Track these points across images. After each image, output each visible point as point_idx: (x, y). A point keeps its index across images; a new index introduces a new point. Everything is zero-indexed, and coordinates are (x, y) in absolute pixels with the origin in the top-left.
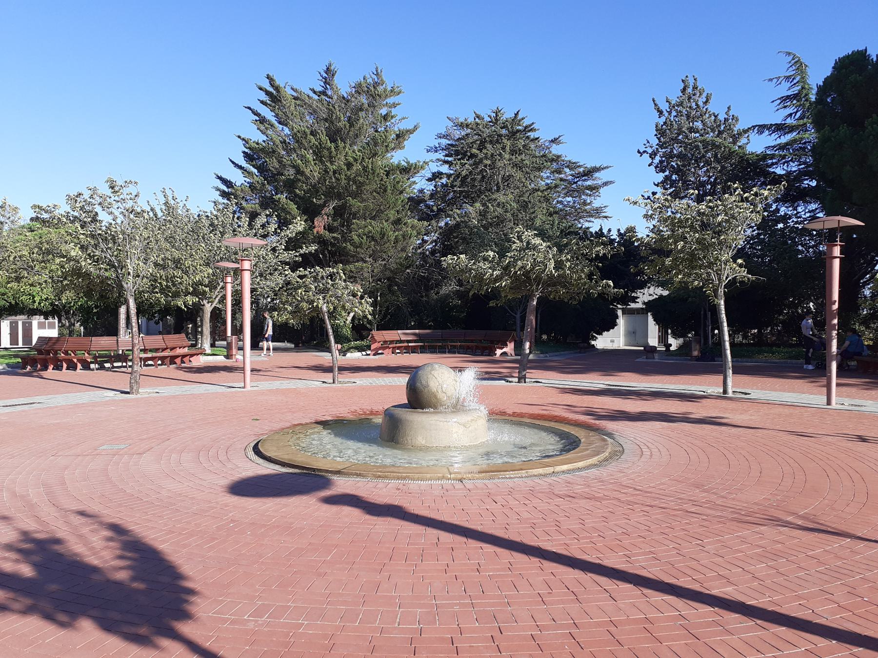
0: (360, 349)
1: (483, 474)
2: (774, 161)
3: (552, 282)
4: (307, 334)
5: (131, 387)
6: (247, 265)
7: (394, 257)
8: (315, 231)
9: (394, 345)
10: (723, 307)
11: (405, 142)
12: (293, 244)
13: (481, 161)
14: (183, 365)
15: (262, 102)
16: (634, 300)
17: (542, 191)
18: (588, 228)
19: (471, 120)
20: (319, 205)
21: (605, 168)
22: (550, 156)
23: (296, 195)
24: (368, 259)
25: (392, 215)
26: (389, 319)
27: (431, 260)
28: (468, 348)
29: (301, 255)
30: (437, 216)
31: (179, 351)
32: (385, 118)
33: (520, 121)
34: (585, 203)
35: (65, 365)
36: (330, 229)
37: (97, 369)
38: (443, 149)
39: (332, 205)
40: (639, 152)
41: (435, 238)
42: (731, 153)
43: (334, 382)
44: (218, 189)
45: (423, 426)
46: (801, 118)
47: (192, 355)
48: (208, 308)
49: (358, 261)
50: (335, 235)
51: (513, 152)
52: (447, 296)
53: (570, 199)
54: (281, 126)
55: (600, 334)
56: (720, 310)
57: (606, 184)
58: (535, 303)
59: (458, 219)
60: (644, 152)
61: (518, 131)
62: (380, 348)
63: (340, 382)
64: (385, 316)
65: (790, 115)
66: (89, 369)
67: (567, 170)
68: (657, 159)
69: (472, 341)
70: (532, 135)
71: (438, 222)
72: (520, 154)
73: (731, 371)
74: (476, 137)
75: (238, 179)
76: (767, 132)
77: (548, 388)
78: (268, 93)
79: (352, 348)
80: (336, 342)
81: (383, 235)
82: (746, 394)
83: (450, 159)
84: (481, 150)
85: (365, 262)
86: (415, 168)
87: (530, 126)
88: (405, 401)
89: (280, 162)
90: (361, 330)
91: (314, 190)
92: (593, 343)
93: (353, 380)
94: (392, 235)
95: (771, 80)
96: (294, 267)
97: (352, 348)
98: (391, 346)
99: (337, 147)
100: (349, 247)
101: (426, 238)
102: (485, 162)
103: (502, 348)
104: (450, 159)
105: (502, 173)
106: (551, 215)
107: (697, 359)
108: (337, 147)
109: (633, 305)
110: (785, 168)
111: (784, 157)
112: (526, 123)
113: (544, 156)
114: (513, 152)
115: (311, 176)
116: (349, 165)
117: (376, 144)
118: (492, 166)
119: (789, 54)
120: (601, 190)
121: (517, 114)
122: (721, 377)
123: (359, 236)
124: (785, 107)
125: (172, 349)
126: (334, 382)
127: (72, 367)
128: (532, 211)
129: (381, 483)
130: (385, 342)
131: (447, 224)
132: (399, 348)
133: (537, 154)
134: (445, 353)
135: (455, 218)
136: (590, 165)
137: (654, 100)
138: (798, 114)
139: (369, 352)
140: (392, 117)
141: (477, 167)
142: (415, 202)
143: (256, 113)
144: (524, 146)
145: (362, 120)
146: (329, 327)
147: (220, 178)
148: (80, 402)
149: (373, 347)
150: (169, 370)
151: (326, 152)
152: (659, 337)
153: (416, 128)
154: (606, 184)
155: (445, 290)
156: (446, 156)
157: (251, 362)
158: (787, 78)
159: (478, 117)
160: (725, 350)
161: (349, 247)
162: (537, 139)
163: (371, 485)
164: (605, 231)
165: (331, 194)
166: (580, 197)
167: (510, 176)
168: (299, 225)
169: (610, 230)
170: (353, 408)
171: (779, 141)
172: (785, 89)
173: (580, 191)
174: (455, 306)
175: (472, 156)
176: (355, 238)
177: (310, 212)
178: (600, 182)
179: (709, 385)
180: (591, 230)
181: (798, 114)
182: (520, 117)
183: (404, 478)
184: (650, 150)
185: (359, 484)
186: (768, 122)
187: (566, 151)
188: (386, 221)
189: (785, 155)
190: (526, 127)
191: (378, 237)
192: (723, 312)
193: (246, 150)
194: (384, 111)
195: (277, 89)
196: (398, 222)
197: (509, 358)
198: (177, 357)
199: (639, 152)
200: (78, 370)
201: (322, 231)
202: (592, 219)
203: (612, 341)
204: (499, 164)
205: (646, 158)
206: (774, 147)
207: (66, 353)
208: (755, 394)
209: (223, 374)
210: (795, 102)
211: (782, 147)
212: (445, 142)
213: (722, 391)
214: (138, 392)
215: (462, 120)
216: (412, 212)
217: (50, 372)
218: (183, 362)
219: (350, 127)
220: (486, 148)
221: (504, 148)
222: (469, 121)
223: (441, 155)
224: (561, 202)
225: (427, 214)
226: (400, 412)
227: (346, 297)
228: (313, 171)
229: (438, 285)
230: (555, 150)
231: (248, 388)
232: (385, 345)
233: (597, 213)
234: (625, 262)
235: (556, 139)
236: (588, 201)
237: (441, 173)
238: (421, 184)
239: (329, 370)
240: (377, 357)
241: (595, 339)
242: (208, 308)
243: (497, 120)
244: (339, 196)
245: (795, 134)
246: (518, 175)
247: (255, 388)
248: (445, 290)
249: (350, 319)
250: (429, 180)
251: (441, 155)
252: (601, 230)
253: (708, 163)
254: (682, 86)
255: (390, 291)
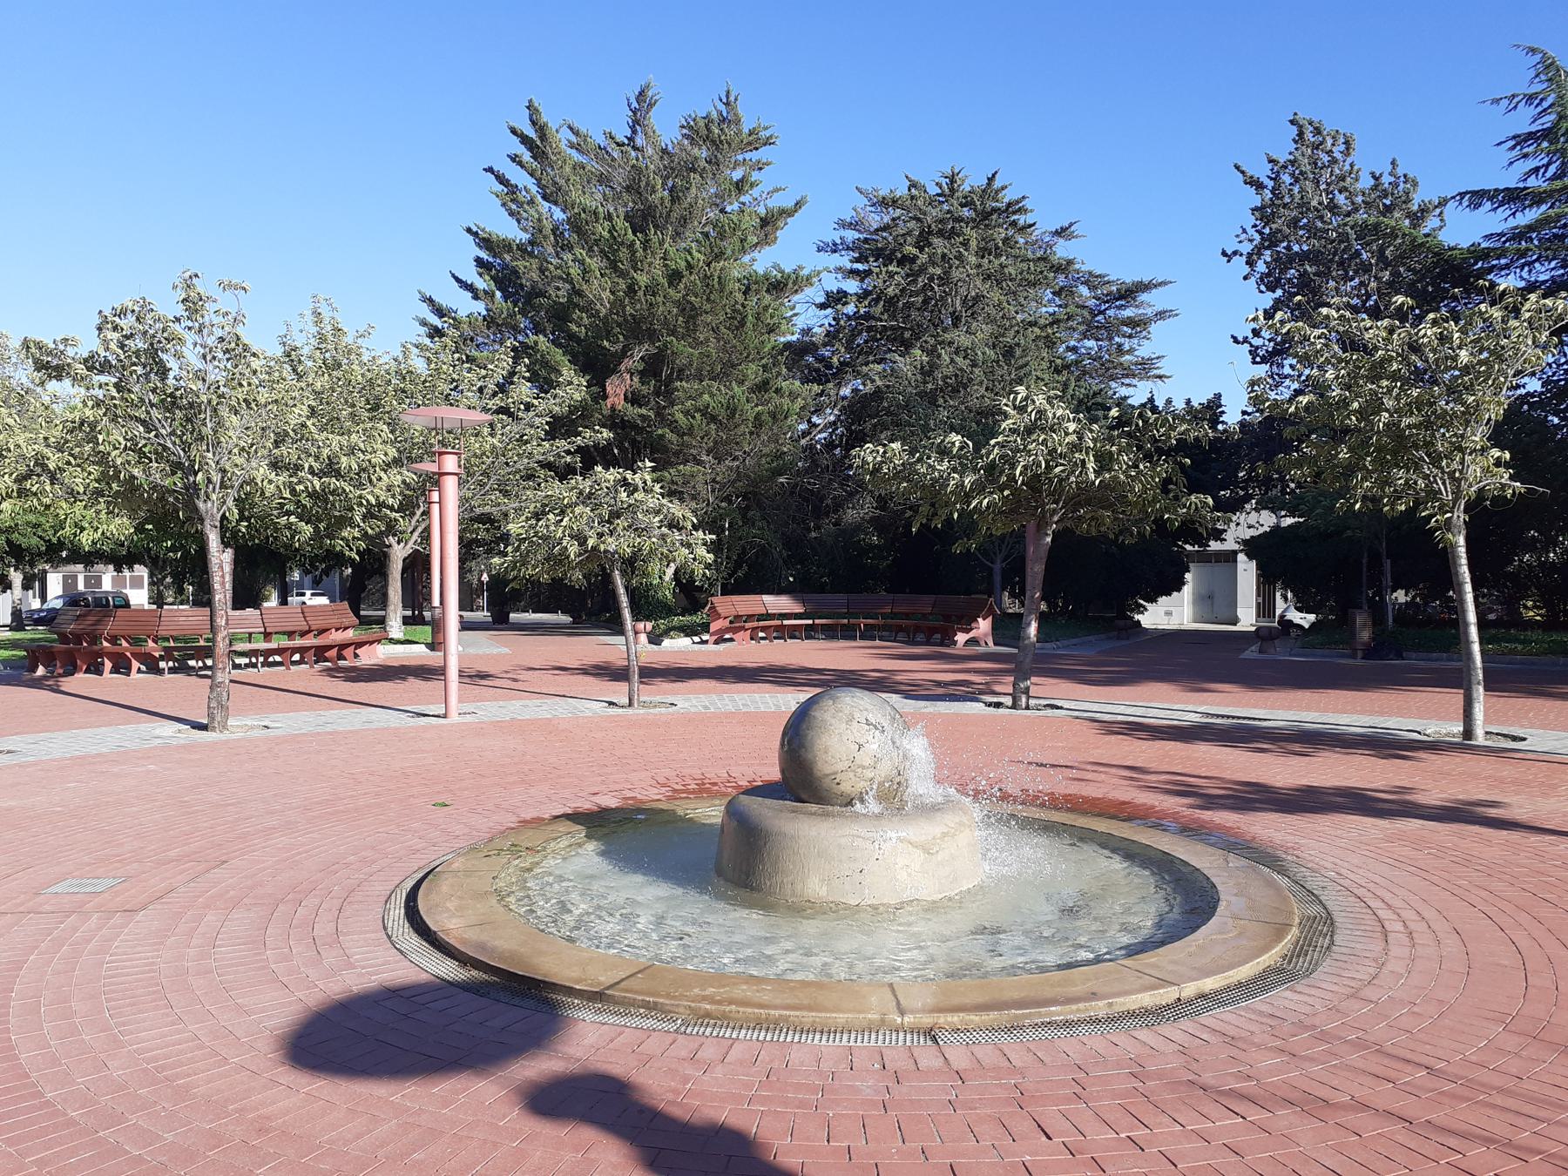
0: (689, 631)
1: (993, 1015)
2: (1503, 261)
3: (1086, 496)
4: (586, 599)
5: (211, 716)
6: (450, 463)
7: (753, 450)
8: (609, 402)
9: (755, 624)
10: (1462, 551)
11: (779, 233)
12: (559, 427)
13: (923, 269)
14: (341, 663)
15: (515, 159)
16: (1218, 535)
17: (1043, 328)
18: (1126, 398)
19: (902, 191)
20: (614, 355)
21: (1160, 284)
22: (1055, 259)
23: (572, 336)
24: (704, 458)
25: (753, 371)
26: (746, 571)
27: (830, 462)
28: (900, 629)
29: (580, 450)
30: (839, 374)
31: (336, 637)
32: (740, 186)
33: (997, 192)
34: (1120, 350)
35: (108, 665)
36: (634, 399)
37: (172, 670)
38: (848, 248)
39: (639, 352)
40: (1224, 254)
41: (832, 418)
42: (1416, 247)
43: (630, 705)
44: (424, 323)
45: (827, 855)
46: (1555, 177)
47: (360, 645)
48: (399, 553)
49: (685, 462)
50: (644, 411)
51: (982, 252)
52: (858, 528)
53: (1091, 343)
54: (546, 204)
55: (1153, 600)
56: (1455, 557)
57: (1161, 315)
58: (1049, 539)
59: (879, 383)
60: (1235, 253)
61: (994, 210)
62: (728, 630)
63: (644, 705)
64: (738, 565)
65: (1537, 170)
66: (160, 672)
67: (1084, 290)
68: (1261, 267)
69: (907, 616)
70: (1022, 220)
71: (839, 385)
72: (998, 256)
73: (1481, 689)
74: (912, 224)
75: (467, 307)
76: (1488, 205)
77: (1070, 722)
78: (525, 140)
79: (673, 628)
80: (637, 617)
81: (732, 410)
82: (1515, 739)
83: (860, 266)
84: (921, 250)
85: (700, 463)
86: (795, 283)
87: (1018, 202)
88: (774, 773)
89: (542, 271)
90: (691, 595)
91: (604, 329)
92: (1137, 617)
93: (670, 699)
94: (750, 410)
95: (1497, 101)
96: (564, 473)
97: (673, 628)
98: (748, 625)
99: (646, 244)
100: (670, 436)
101: (815, 419)
102: (931, 270)
103: (967, 631)
104: (860, 266)
105: (963, 291)
106: (1057, 371)
107: (1371, 652)
108: (646, 244)
109: (1214, 546)
110: (1525, 274)
111: (1523, 254)
112: (1008, 196)
113: (1043, 259)
114: (982, 252)
115: (600, 296)
116: (674, 277)
117: (722, 236)
118: (945, 279)
119: (1533, 51)
120: (1153, 328)
121: (991, 180)
122: (1455, 697)
123: (686, 413)
124: (1525, 156)
125: (322, 632)
126: (630, 705)
127: (122, 666)
128: (1021, 362)
129: (710, 1040)
130: (738, 617)
131: (855, 391)
132: (763, 629)
133: (1030, 255)
134: (854, 638)
135: (873, 381)
136: (1129, 278)
137: (1237, 167)
138: (1552, 169)
139: (706, 637)
140: (752, 185)
141: (915, 281)
142: (799, 351)
143: (501, 179)
144: (1006, 240)
145: (693, 190)
146: (622, 590)
147: (430, 301)
148: (93, 750)
149: (714, 627)
150: (304, 675)
151: (624, 253)
152: (1258, 604)
153: (799, 205)
154: (1161, 315)
155: (851, 515)
156: (857, 260)
157: (461, 657)
158: (1530, 98)
159: (913, 185)
160: (1468, 643)
161: (670, 436)
162: (1031, 226)
163: (683, 1047)
164: (1160, 403)
165: (638, 330)
166: (1111, 339)
167: (978, 298)
168: (573, 387)
169: (1169, 401)
170: (664, 773)
171: (1512, 223)
172: (1524, 120)
173: (1110, 329)
174: (872, 547)
175: (905, 260)
176: (679, 416)
177: (597, 367)
178: (1149, 312)
179: (1420, 713)
180: (1130, 401)
181: (1552, 169)
182: (997, 184)
183: (773, 1025)
184: (1246, 248)
185: (653, 1045)
186: (1489, 185)
187: (1085, 254)
188: (741, 383)
189: (1528, 249)
190: (1009, 205)
191: (723, 415)
192: (1464, 561)
193: (484, 255)
194: (737, 175)
195: (542, 130)
196: (763, 387)
197: (981, 649)
198: (331, 647)
199: (1224, 254)
200: (134, 675)
201: (620, 404)
202: (1134, 382)
203: (1168, 614)
204: (956, 274)
205: (1240, 263)
206: (1501, 235)
207: (114, 640)
208: (1539, 739)
209: (414, 683)
210: (1545, 144)
211: (1520, 234)
212: (851, 235)
213: (1459, 728)
214: (225, 727)
215: (883, 192)
216: (789, 370)
217: (80, 681)
218: (341, 657)
219: (673, 201)
220: (930, 244)
221: (965, 244)
222: (898, 194)
223: (844, 260)
224: (1074, 349)
225: (817, 370)
226: (767, 811)
227: (659, 522)
228: (601, 291)
229: (838, 505)
230: (1062, 250)
231: (454, 717)
232: (737, 623)
233: (1145, 368)
234: (1214, 459)
235: (1064, 230)
236: (1127, 347)
237: (845, 294)
238: (806, 316)
239: (617, 674)
240: (722, 646)
241: (1141, 609)
242: (399, 553)
243: (952, 190)
244: (652, 336)
245: (1544, 207)
246: (995, 296)
247: (469, 718)
248: (851, 515)
249: (670, 571)
250: (822, 306)
251: (844, 260)
252: (1151, 400)
253: (1365, 268)
254: (1294, 130)
255: (744, 517)
